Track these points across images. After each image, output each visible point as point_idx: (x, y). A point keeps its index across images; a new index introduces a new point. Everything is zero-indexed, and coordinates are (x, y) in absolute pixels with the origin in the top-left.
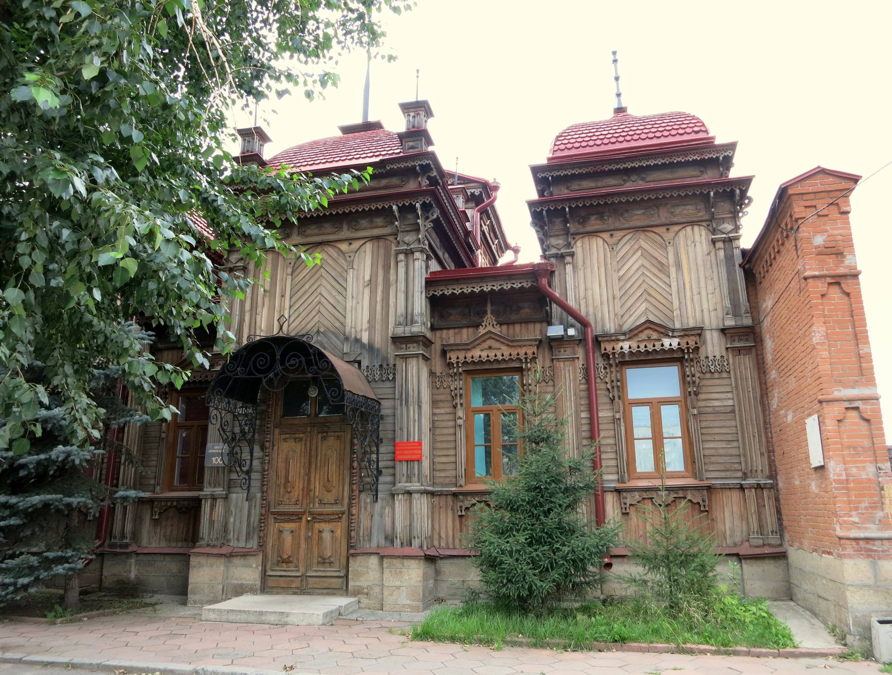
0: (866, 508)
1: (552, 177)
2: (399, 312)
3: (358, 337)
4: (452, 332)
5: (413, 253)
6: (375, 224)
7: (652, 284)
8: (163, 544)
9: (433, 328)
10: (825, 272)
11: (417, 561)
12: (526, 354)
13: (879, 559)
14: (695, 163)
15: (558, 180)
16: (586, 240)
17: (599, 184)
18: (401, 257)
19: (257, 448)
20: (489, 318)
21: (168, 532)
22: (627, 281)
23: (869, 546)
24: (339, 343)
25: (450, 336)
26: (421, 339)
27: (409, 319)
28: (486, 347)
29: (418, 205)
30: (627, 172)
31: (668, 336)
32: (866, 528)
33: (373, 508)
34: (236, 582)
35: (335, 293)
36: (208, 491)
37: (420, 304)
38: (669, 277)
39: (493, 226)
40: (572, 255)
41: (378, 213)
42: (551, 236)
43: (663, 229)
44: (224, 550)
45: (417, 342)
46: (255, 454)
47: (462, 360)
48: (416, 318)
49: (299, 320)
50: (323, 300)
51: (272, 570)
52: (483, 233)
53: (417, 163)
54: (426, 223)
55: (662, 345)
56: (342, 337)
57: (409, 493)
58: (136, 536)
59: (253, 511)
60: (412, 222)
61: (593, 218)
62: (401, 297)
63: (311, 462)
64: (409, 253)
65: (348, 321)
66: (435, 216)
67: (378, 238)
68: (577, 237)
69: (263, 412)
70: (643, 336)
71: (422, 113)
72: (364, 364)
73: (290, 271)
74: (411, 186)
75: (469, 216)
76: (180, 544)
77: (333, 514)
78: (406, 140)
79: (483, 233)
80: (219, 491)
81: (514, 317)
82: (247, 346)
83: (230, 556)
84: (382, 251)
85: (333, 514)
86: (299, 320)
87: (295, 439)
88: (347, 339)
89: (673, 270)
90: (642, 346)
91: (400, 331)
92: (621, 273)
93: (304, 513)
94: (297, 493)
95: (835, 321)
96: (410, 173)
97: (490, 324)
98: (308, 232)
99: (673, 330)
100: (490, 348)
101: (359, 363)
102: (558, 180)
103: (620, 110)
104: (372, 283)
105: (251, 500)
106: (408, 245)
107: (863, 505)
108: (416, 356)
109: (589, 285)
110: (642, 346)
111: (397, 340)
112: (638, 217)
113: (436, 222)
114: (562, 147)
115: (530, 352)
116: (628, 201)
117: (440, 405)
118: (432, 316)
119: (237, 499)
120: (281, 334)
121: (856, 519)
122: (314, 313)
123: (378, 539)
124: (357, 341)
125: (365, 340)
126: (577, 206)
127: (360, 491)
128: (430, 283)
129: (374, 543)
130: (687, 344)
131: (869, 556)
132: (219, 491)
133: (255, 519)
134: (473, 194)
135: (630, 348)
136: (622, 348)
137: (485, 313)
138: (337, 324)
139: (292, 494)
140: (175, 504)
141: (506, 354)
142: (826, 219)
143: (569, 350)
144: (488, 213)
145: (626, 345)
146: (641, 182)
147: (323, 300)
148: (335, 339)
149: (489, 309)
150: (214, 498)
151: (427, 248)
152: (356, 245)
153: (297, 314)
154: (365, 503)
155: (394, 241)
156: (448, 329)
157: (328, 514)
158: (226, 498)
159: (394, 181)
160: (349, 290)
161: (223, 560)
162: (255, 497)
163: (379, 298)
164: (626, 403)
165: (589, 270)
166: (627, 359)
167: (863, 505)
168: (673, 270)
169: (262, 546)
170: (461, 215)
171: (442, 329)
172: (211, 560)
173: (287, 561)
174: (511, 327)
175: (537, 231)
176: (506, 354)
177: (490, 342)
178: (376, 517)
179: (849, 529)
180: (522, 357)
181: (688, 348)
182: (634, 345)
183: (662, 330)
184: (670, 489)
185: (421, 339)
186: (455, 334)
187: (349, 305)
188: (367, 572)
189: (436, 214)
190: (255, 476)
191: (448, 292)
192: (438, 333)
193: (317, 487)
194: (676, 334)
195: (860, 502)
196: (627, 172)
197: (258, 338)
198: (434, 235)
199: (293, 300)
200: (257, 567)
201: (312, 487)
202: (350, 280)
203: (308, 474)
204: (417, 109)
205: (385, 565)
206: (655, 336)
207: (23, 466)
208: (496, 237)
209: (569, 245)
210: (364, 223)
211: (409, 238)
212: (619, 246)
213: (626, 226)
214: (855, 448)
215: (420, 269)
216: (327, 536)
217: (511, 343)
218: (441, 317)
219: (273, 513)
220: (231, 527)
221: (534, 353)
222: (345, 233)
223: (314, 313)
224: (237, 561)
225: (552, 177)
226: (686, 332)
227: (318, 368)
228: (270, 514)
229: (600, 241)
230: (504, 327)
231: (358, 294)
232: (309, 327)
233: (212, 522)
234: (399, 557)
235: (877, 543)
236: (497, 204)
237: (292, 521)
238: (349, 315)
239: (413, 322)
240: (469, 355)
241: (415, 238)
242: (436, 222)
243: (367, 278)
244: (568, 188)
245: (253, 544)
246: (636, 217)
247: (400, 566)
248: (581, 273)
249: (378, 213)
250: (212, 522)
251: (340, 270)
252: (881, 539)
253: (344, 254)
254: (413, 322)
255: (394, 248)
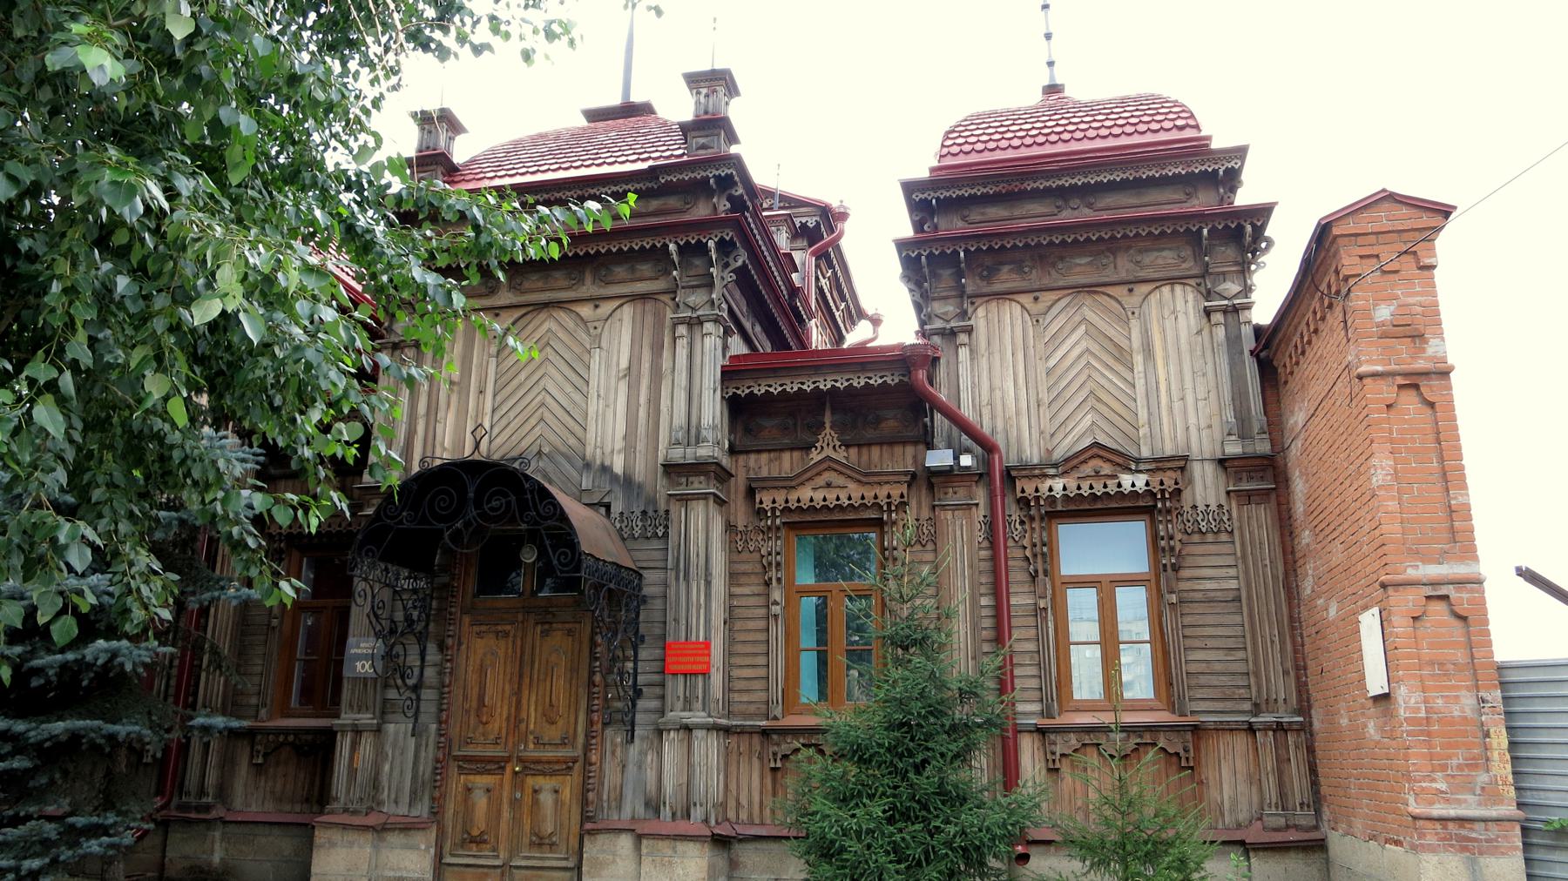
0: (1460, 767)
1: (938, 199)
2: (676, 422)
3: (607, 463)
4: (764, 457)
5: (701, 323)
6: (638, 275)
7: (1103, 381)
8: (269, 806)
9: (733, 451)
10: (1393, 367)
11: (698, 845)
12: (889, 496)
13: (1481, 853)
14: (1176, 180)
15: (948, 205)
16: (994, 304)
17: (1017, 213)
18: (682, 330)
19: (432, 648)
20: (828, 435)
21: (279, 787)
22: (1060, 378)
23: (1464, 832)
24: (575, 473)
25: (762, 465)
26: (713, 468)
27: (692, 435)
28: (822, 483)
29: (711, 244)
30: (1064, 194)
31: (1128, 470)
32: (1459, 802)
33: (625, 752)
34: (391, 874)
35: (569, 389)
36: (347, 718)
37: (712, 410)
38: (1132, 370)
39: (837, 279)
40: (969, 331)
41: (644, 255)
42: (934, 299)
43: (1123, 290)
44: (372, 820)
45: (706, 474)
46: (428, 658)
47: (781, 504)
48: (704, 433)
49: (508, 432)
50: (549, 400)
51: (453, 855)
52: (820, 290)
53: (711, 173)
54: (725, 274)
55: (1119, 485)
56: (580, 463)
57: (688, 729)
58: (223, 792)
59: (423, 754)
60: (701, 272)
61: (1006, 269)
62: (681, 396)
63: (522, 673)
64: (694, 323)
65: (591, 436)
66: (740, 263)
67: (644, 297)
68: (978, 301)
69: (445, 586)
70: (1087, 469)
71: (721, 90)
72: (616, 508)
73: (493, 350)
74: (701, 211)
75: (797, 262)
76: (298, 808)
77: (558, 762)
78: (694, 134)
79: (820, 290)
80: (366, 719)
81: (870, 434)
82: (419, 476)
83: (381, 830)
84: (649, 319)
85: (558, 762)
86: (508, 432)
87: (497, 633)
88: (588, 466)
89: (1138, 359)
90: (1085, 486)
91: (677, 455)
92: (1052, 362)
93: (508, 760)
94: (497, 725)
95: (1409, 450)
96: (700, 189)
97: (828, 446)
98: (527, 285)
99: (1138, 461)
100: (829, 485)
101: (608, 507)
102: (948, 205)
103: (1052, 89)
104: (631, 373)
105: (420, 736)
106: (693, 309)
107: (1455, 762)
108: (705, 497)
109: (997, 382)
110: (1085, 486)
111: (672, 470)
112: (1081, 269)
113: (742, 272)
114: (955, 149)
115: (896, 493)
116: (1063, 242)
117: (743, 580)
118: (732, 430)
119: (397, 733)
120: (476, 457)
121: (1442, 786)
122: (533, 421)
123: (633, 806)
124: (605, 469)
125: (618, 468)
126: (979, 250)
127: (605, 725)
128: (729, 374)
129: (627, 813)
130: (1162, 483)
131: (1464, 849)
132: (366, 719)
133: (426, 768)
134: (804, 225)
135: (1065, 488)
136: (1051, 489)
137: (822, 426)
138: (572, 441)
139: (490, 726)
140: (291, 738)
141: (856, 495)
142: (1396, 277)
143: (962, 492)
144: (829, 257)
145: (1058, 485)
146: (1087, 211)
147: (549, 400)
148: (568, 466)
149: (828, 420)
150: (357, 731)
151: (725, 315)
152: (606, 308)
153: (504, 422)
154: (614, 744)
155: (671, 303)
156: (759, 452)
157: (549, 762)
158: (378, 731)
159: (673, 202)
160: (593, 383)
161: (369, 836)
162: (427, 729)
163: (643, 399)
164: (1058, 583)
165: (997, 356)
166: (1059, 508)
167: (1455, 762)
168: (1138, 359)
169: (436, 813)
170: (784, 261)
171: (748, 452)
172: (351, 836)
173: (478, 841)
174: (865, 450)
175: (911, 290)
176: (856, 495)
177: (829, 476)
178: (631, 768)
179: (1431, 803)
180: (883, 502)
181: (1163, 491)
182: (1072, 483)
183: (1120, 460)
184: (1129, 730)
185: (713, 468)
186: (771, 460)
187: (592, 410)
188: (614, 861)
189: (741, 258)
190: (428, 694)
191: (759, 390)
192: (742, 459)
193: (532, 714)
194: (1142, 467)
195: (1449, 757)
196: (1064, 194)
197: (438, 462)
198: (738, 294)
199: (499, 398)
200: (427, 849)
201: (524, 715)
202: (594, 366)
203: (518, 693)
204: (713, 82)
205: (644, 851)
206: (1107, 469)
207: (39, 671)
208: (843, 299)
209: (964, 315)
210: (620, 271)
211: (697, 298)
212: (1049, 318)
213: (1061, 283)
214: (1441, 664)
215: (712, 350)
216: (546, 799)
217: (864, 477)
218: (748, 431)
219: (456, 758)
220: (385, 783)
221: (902, 496)
222: (589, 288)
223: (533, 421)
224: (394, 838)
225: (938, 199)
226: (1160, 464)
227: (539, 514)
228: (452, 759)
229: (1017, 309)
230: (853, 451)
231: (608, 389)
232: (525, 444)
233: (352, 772)
234: (668, 837)
235: (1477, 826)
236: (844, 243)
237: (489, 772)
238: (591, 428)
239: (699, 440)
240: (793, 497)
241: (705, 298)
242: (742, 272)
243: (624, 364)
244: (964, 219)
245: (422, 810)
246: (1078, 269)
247: (670, 852)
248: (984, 362)
249: (644, 255)
250: (352, 772)
251: (578, 350)
252: (1485, 820)
253: (585, 322)
254: (699, 440)
255: (670, 315)
